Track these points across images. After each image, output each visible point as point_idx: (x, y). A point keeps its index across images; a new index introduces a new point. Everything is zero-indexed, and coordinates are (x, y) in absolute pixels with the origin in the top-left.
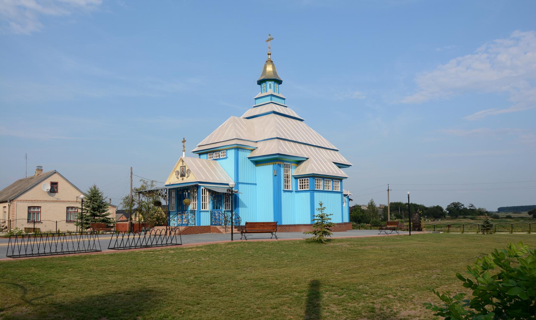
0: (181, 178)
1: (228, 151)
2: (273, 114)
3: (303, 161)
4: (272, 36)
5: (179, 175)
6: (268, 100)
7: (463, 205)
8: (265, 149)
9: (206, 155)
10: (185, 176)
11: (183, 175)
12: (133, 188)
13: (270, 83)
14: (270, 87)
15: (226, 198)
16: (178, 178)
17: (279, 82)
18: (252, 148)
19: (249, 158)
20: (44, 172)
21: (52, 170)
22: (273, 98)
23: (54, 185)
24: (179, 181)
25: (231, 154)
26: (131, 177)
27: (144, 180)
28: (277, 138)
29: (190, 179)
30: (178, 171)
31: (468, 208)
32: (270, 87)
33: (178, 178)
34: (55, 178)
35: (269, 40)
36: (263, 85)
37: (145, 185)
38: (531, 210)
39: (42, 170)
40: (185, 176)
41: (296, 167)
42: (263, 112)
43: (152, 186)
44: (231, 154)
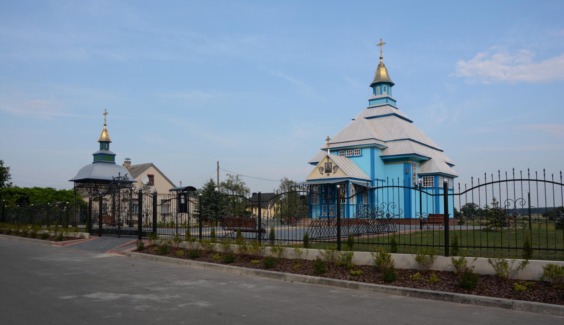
0: (327, 174)
1: (363, 150)
2: (394, 116)
3: (427, 160)
4: (383, 41)
5: (324, 172)
6: (384, 102)
7: (477, 206)
8: (394, 150)
9: (336, 153)
10: (331, 172)
11: (328, 171)
12: (220, 182)
13: (384, 86)
14: (385, 90)
15: (365, 191)
16: (322, 174)
17: (391, 84)
18: (382, 147)
19: (381, 157)
20: (132, 164)
21: (149, 162)
22: (389, 100)
23: (151, 177)
24: (325, 176)
25: (367, 153)
26: (218, 171)
27: (230, 173)
28: (409, 139)
29: (338, 175)
30: (322, 168)
31: (483, 209)
32: (385, 90)
33: (322, 174)
34: (151, 171)
35: (381, 45)
36: (378, 88)
37: (231, 179)
38: (544, 212)
39: (130, 162)
40: (331, 172)
41: (420, 166)
42: (381, 114)
43: (238, 180)
44: (367, 153)
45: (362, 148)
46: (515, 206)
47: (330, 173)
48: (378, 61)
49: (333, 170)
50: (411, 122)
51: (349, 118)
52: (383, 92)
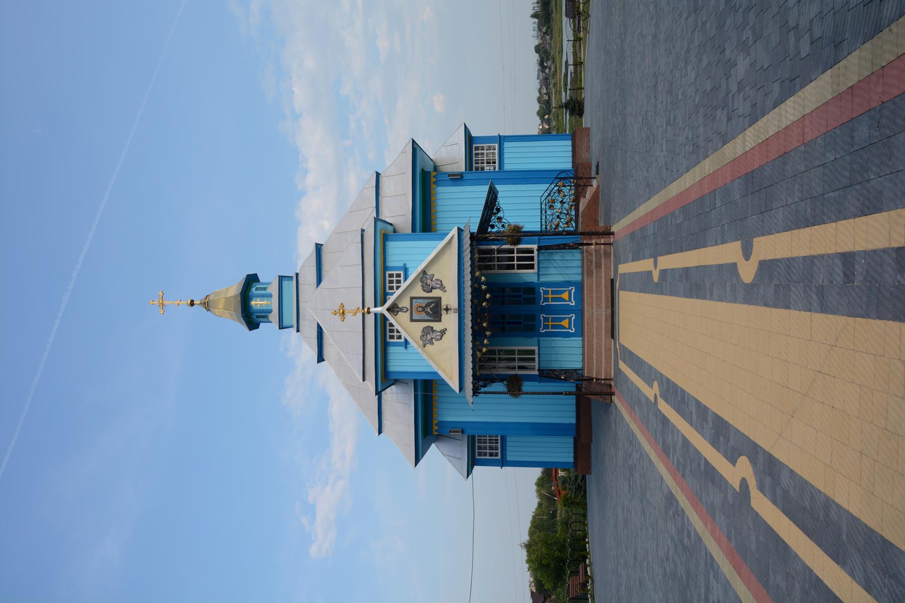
0: (444, 316)
1: (390, 264)
5: (437, 326)
10: (438, 300)
11: (435, 310)
14: (265, 289)
24: (450, 321)
30: (428, 331)
32: (265, 289)
33: (443, 332)
45: (385, 268)
46: (570, 394)
47: (444, 303)
48: (199, 309)
49: (436, 293)
50: (380, 432)
51: (324, 413)
52: (268, 291)
